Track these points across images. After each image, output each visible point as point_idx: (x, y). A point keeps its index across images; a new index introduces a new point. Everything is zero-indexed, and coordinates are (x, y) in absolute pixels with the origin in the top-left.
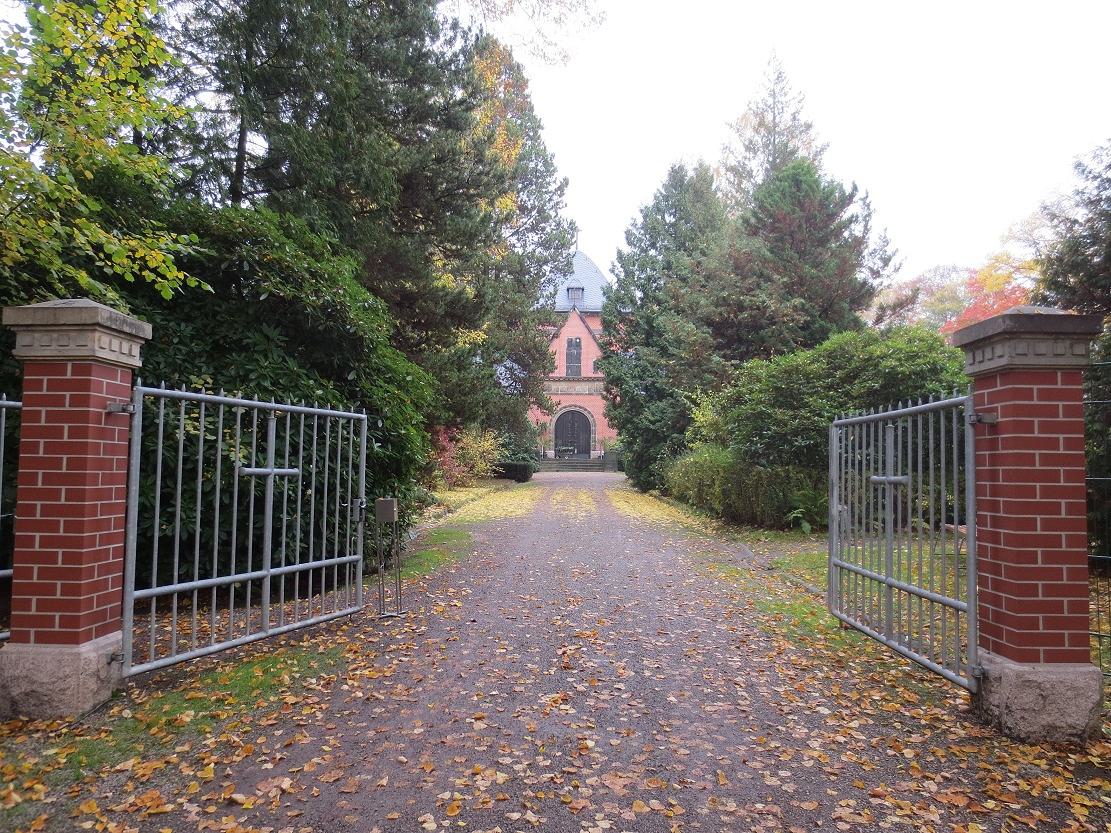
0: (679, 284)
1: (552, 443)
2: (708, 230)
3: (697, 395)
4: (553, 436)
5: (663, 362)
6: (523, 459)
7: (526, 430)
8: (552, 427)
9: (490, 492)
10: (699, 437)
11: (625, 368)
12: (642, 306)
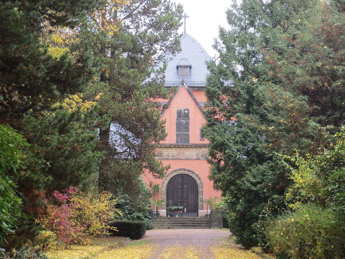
0: (276, 56)
1: (164, 203)
2: (300, 9)
3: (296, 158)
4: (164, 197)
5: (263, 128)
6: (138, 218)
7: (139, 192)
8: (163, 189)
9: (103, 251)
10: (298, 197)
11: (228, 135)
12: (243, 79)
